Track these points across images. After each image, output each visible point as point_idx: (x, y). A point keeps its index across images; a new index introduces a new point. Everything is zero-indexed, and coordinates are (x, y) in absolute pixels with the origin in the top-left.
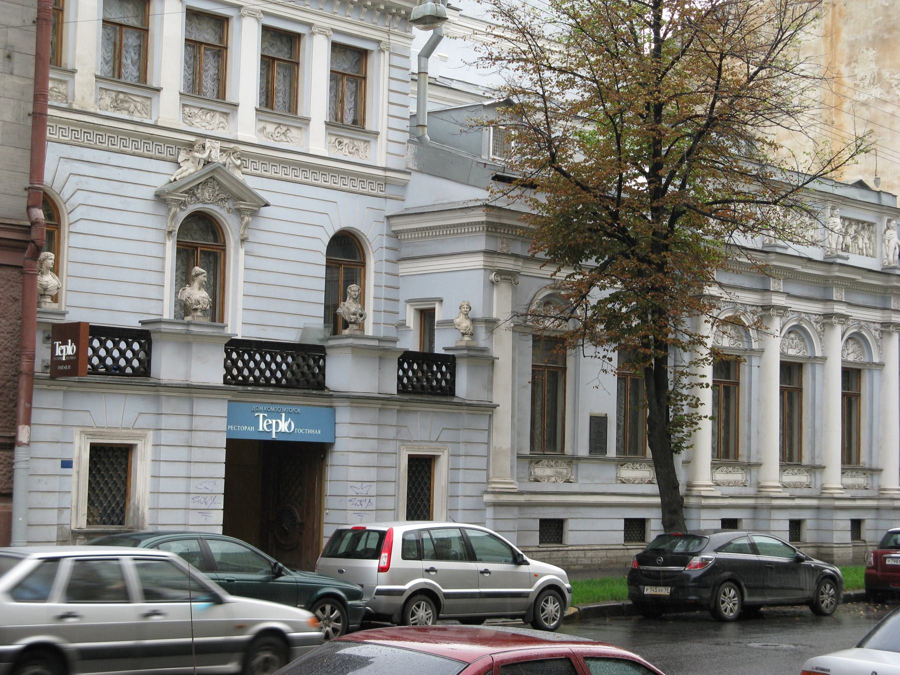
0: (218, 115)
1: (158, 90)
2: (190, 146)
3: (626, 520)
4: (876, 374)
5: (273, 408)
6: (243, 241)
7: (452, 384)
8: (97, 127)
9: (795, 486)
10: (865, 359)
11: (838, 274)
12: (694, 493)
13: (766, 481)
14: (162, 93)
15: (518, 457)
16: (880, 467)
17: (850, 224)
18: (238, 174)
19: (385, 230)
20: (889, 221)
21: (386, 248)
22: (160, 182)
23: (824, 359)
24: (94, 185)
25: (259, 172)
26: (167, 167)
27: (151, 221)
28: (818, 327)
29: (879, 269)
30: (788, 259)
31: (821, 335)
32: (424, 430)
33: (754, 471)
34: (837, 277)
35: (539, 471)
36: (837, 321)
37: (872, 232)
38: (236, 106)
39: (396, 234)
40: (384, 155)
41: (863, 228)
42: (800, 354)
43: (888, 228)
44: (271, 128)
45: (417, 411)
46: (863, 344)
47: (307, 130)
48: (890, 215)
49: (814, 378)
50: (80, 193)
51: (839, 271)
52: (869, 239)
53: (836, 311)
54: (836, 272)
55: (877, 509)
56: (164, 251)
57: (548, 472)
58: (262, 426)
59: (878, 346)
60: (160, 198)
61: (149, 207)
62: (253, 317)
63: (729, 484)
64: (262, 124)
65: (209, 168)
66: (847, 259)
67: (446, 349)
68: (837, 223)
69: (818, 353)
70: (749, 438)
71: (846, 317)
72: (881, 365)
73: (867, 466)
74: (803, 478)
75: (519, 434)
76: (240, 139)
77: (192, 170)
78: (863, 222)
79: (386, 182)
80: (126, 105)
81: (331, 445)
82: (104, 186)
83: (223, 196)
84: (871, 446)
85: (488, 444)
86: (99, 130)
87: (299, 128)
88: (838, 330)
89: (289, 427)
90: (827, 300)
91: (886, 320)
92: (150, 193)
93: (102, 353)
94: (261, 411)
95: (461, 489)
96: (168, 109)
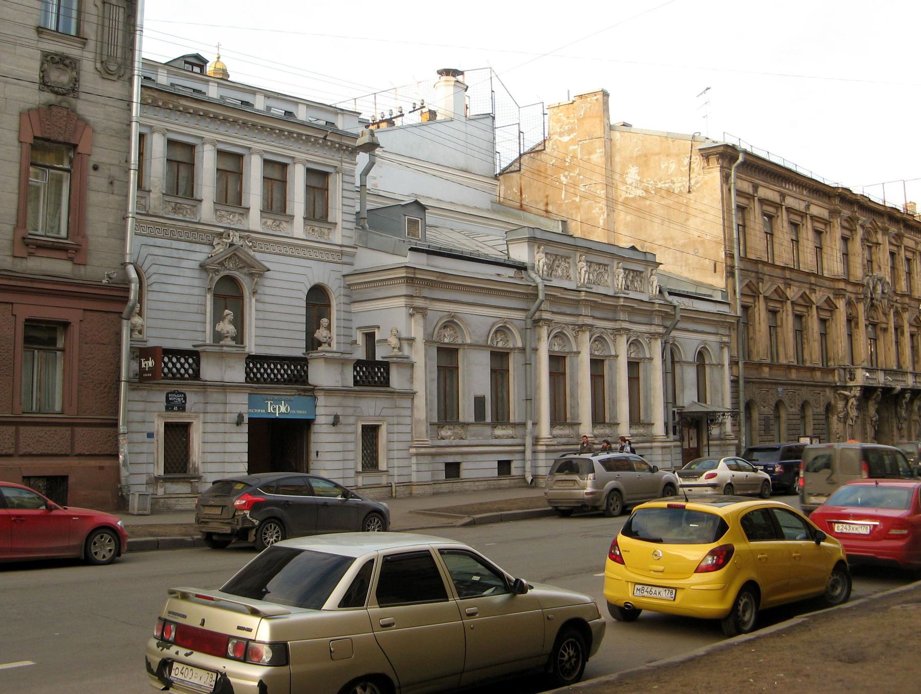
1: (201, 201)
2: (220, 235)
5: (276, 398)
10: (641, 356)
14: (203, 203)
22: (202, 257)
26: (206, 249)
27: (196, 282)
44: (270, 222)
57: (449, 433)
58: (270, 409)
60: (203, 267)
61: (196, 274)
64: (264, 220)
65: (233, 248)
67: (383, 358)
71: (629, 330)
72: (651, 359)
81: (313, 420)
83: (241, 265)
85: (411, 416)
89: (287, 409)
90: (615, 320)
92: (196, 265)
96: (206, 211)
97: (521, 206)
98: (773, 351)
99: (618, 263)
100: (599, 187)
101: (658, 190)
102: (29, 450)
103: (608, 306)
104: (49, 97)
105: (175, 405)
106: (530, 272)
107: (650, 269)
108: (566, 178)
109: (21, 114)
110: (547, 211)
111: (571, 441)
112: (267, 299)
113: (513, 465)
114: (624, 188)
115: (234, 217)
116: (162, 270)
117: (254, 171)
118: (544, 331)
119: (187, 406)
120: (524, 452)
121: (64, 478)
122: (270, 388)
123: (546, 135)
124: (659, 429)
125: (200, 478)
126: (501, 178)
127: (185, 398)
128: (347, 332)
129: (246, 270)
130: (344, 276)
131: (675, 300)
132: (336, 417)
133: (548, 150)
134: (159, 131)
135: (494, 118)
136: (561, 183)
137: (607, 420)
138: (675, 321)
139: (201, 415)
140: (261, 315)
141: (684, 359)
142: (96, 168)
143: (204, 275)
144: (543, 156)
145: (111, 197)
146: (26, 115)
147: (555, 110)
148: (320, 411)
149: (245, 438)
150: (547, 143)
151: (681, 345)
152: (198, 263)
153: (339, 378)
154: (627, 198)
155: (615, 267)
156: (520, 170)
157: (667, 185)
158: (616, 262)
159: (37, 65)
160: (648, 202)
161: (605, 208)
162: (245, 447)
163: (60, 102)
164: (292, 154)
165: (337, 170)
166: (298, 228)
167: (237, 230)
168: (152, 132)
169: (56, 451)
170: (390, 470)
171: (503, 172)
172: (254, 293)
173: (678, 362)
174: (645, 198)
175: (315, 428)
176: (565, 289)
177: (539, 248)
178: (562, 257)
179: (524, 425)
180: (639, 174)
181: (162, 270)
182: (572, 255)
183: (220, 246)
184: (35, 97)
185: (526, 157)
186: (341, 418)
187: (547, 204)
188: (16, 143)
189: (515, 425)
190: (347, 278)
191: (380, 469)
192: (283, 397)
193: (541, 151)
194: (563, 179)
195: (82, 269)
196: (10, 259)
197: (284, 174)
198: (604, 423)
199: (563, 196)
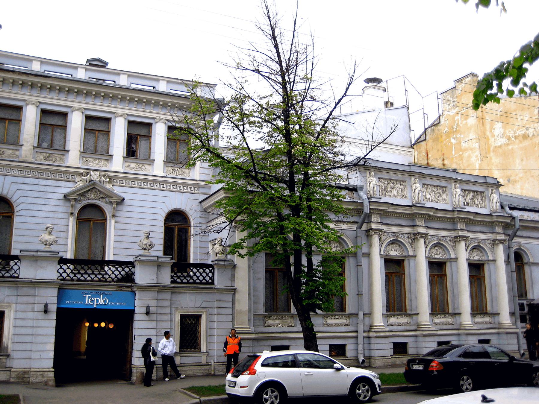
0: (103, 161)
1: (68, 151)
2: (81, 174)
3: (330, 345)
4: (454, 264)
5: (94, 292)
6: (114, 216)
7: (212, 279)
8: (32, 168)
9: (443, 324)
10: (485, 258)
11: (496, 220)
12: (373, 330)
13: (421, 322)
14: (70, 152)
15: (254, 315)
16: (498, 312)
17: (469, 193)
18: (109, 186)
19: (199, 208)
20: (492, 190)
21: (200, 217)
22: (66, 191)
23: (456, 259)
24: (30, 194)
25: (44, 177)
26: (70, 184)
27: (61, 209)
28: (451, 243)
29: (489, 213)
30: (381, 205)
31: (454, 247)
32: (190, 302)
33: (414, 317)
34: (498, 222)
35: (270, 321)
36: (373, 233)
37: (483, 196)
38: (112, 156)
39: (205, 210)
40: (198, 174)
41: (478, 195)
42: (443, 257)
43: (492, 193)
44: (133, 165)
45: (453, 292)
46: (483, 251)
47: (153, 165)
48: (492, 187)
49: (452, 269)
50: (22, 198)
51: (458, 214)
52: (482, 199)
53: (460, 234)
54: (456, 215)
55: (498, 334)
56: (68, 222)
57: (277, 322)
58: (88, 301)
59: (492, 251)
60: (66, 197)
61: (61, 203)
62: (118, 252)
63: (398, 324)
64: (127, 164)
65: (92, 182)
66: (465, 208)
67: (212, 262)
68: (459, 191)
69: (453, 256)
70: (411, 300)
71: (467, 237)
72: (494, 261)
73: (491, 312)
74: (449, 320)
75: (255, 303)
76: (112, 170)
77: (81, 185)
78: (477, 192)
79: (199, 186)
80: (51, 159)
81: (134, 310)
82: (36, 194)
83: (101, 196)
84: (492, 302)
85: (233, 308)
86: (33, 169)
87: (149, 164)
88: (422, 241)
89: (105, 301)
90: (454, 230)
91: (494, 238)
92: (61, 196)
93: (204, 274)
94: (87, 294)
95: (215, 332)
96: (73, 158)
97: (428, 163)
99: (455, 185)
100: (474, 141)
101: (516, 137)
103: (453, 219)
106: (359, 191)
107: (490, 190)
108: (454, 139)
110: (444, 165)
111: (408, 328)
112: (122, 220)
113: (348, 348)
114: (493, 139)
115: (99, 162)
116: (30, 200)
117: (76, 123)
118: (375, 238)
120: (356, 337)
122: (103, 285)
123: (441, 112)
124: (506, 318)
125: (8, 356)
126: (415, 147)
128: (203, 245)
129: (107, 199)
130: (201, 202)
131: (515, 213)
132: (148, 308)
133: (442, 121)
134: (32, 103)
135: (408, 108)
136: (451, 143)
137: (450, 311)
138: (515, 229)
139: (14, 306)
140: (120, 233)
141: (532, 260)
143: (68, 204)
144: (439, 127)
147: (445, 94)
148: (137, 302)
149: (54, 323)
150: (441, 118)
151: (528, 249)
152: (63, 195)
153: (154, 277)
154: (495, 147)
155: (453, 188)
156: (425, 140)
157: (523, 132)
158: (453, 184)
160: (510, 147)
161: (479, 157)
162: (53, 331)
164: (153, 115)
166: (158, 168)
167: (97, 170)
168: (27, 105)
170: (209, 351)
171: (417, 142)
172: (114, 216)
173: (527, 263)
174: (508, 144)
175: (136, 317)
176: (392, 204)
177: (370, 173)
178: (397, 181)
179: (357, 315)
180: (503, 128)
181: (30, 200)
182: (407, 180)
183: (81, 182)
185: (429, 130)
186: (151, 308)
187: (443, 160)
189: (349, 316)
190: (203, 204)
191: (202, 351)
192: (103, 292)
193: (438, 124)
194: (453, 141)
197: (150, 131)
198: (448, 313)
199: (453, 153)
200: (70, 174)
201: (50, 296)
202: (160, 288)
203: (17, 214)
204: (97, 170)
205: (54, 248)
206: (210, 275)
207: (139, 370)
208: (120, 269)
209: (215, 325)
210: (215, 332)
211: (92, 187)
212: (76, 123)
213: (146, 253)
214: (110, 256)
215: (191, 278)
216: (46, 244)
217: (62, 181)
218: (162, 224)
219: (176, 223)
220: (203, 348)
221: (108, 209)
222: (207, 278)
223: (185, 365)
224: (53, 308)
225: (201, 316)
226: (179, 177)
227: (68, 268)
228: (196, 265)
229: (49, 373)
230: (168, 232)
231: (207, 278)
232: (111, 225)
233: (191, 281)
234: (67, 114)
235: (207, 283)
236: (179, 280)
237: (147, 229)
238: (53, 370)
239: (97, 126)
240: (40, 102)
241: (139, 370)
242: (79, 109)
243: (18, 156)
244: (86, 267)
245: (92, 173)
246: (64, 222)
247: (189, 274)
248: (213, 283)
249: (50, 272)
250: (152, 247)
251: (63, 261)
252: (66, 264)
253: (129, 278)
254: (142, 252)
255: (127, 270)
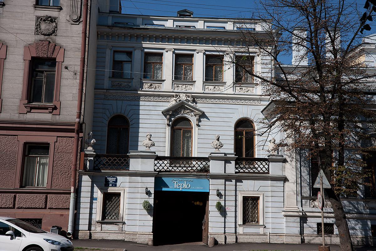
93: (261, 166)
96: (167, 86)
98: (183, 154)
102: (21, 205)
104: (42, 37)
105: (111, 183)
109: (25, 47)
117: (199, 62)
119: (118, 184)
121: (256, 199)
127: (116, 180)
140: (202, 137)
142: (66, 68)
145: (75, 81)
146: (28, 47)
152: (161, 111)
159: (34, 23)
163: (47, 39)
165: (135, 48)
167: (184, 93)
168: (135, 50)
169: (37, 206)
184: (32, 38)
188: (22, 61)
195: (57, 117)
196: (17, 115)
197: (161, 59)
200: (166, 96)
201: (150, 182)
202: (227, 178)
203: (132, 126)
204: (184, 93)
205: (152, 149)
206: (267, 166)
207: (212, 236)
208: (199, 163)
209: (270, 204)
210: (270, 210)
211: (181, 106)
212: (199, 62)
213: (217, 151)
214: (195, 154)
215: (257, 169)
216: (147, 147)
217: (161, 102)
218: (233, 130)
219: (244, 127)
220: (261, 223)
221: (193, 120)
222: (264, 169)
223: (248, 234)
224: (152, 191)
225: (259, 197)
226: (246, 93)
227: (197, 163)
228: (259, 160)
229: (150, 236)
230: (237, 134)
231: (264, 169)
232: (195, 131)
233: (256, 171)
234: (132, 52)
235: (264, 173)
236: (242, 171)
237: (218, 133)
238: (152, 234)
239: (183, 62)
240: (112, 46)
241: (212, 236)
242: (201, 51)
243: (130, 87)
244: (185, 163)
245: (181, 95)
246: (162, 131)
247: (254, 166)
248: (268, 173)
249: (149, 166)
250: (221, 147)
251: (158, 158)
252: (161, 160)
253: (206, 170)
254: (214, 150)
255: (204, 163)
